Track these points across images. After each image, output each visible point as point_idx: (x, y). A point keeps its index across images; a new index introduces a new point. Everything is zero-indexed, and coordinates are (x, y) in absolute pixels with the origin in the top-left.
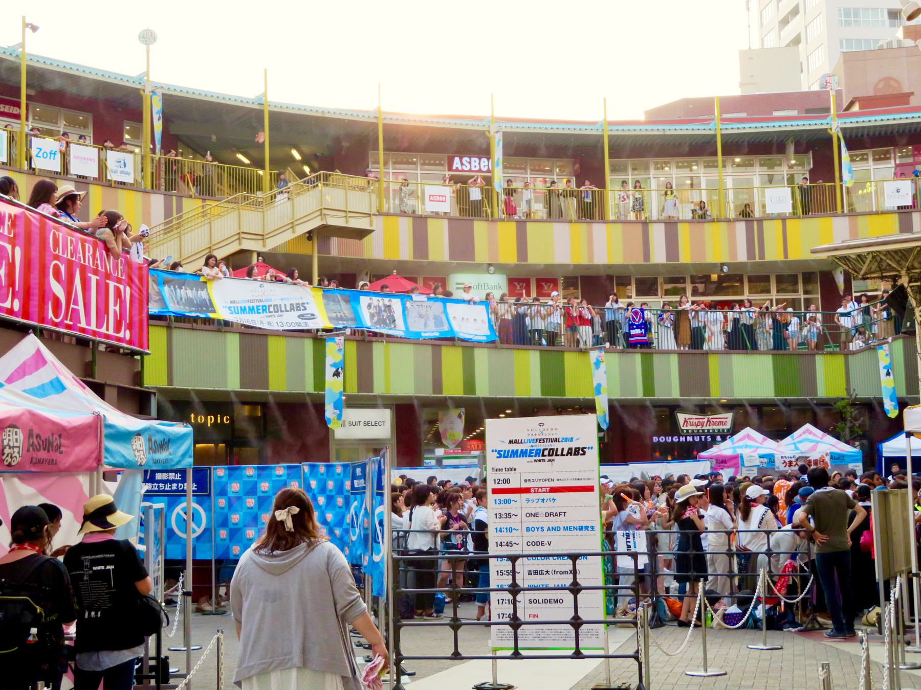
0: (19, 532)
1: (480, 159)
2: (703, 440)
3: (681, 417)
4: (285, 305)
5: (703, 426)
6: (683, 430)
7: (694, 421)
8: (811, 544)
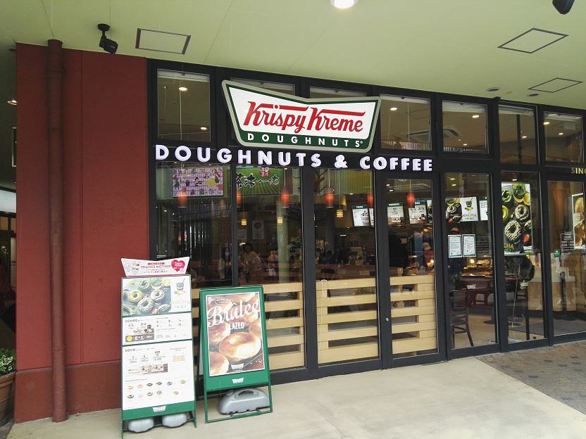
0: (8, 304)
1: (564, 309)
2: (301, 163)
3: (241, 100)
4: (415, 319)
5: (301, 127)
6: (244, 134)
7: (278, 112)
8: (171, 311)
